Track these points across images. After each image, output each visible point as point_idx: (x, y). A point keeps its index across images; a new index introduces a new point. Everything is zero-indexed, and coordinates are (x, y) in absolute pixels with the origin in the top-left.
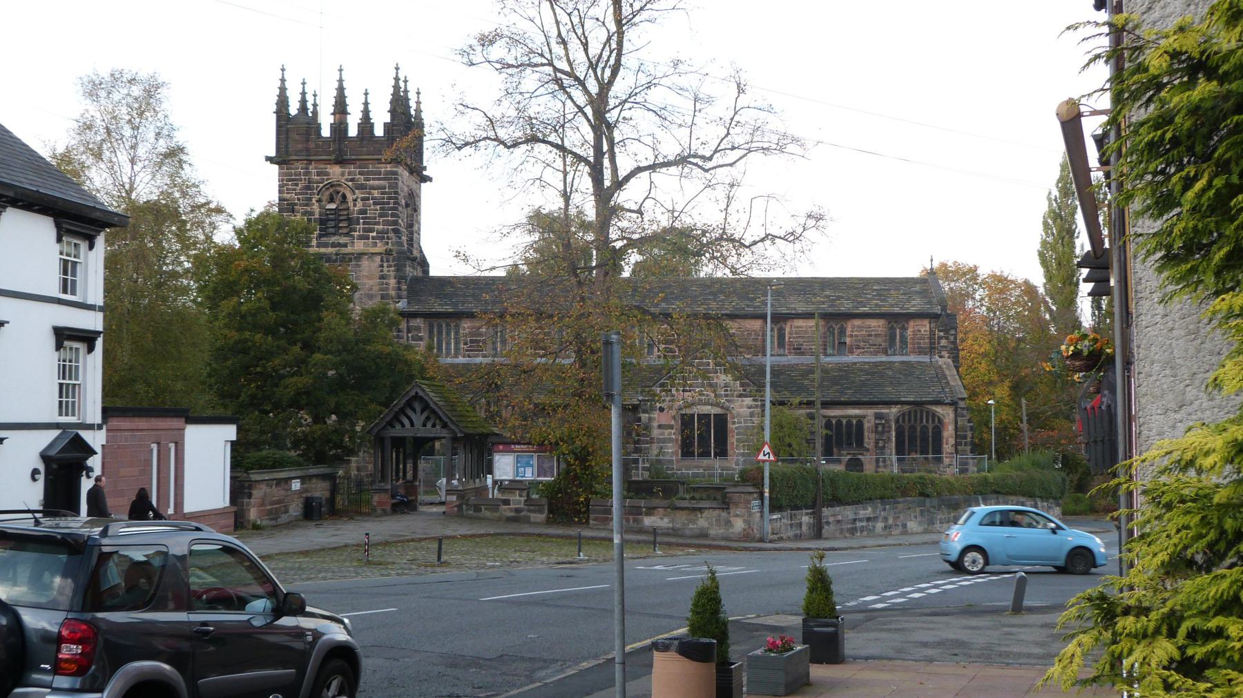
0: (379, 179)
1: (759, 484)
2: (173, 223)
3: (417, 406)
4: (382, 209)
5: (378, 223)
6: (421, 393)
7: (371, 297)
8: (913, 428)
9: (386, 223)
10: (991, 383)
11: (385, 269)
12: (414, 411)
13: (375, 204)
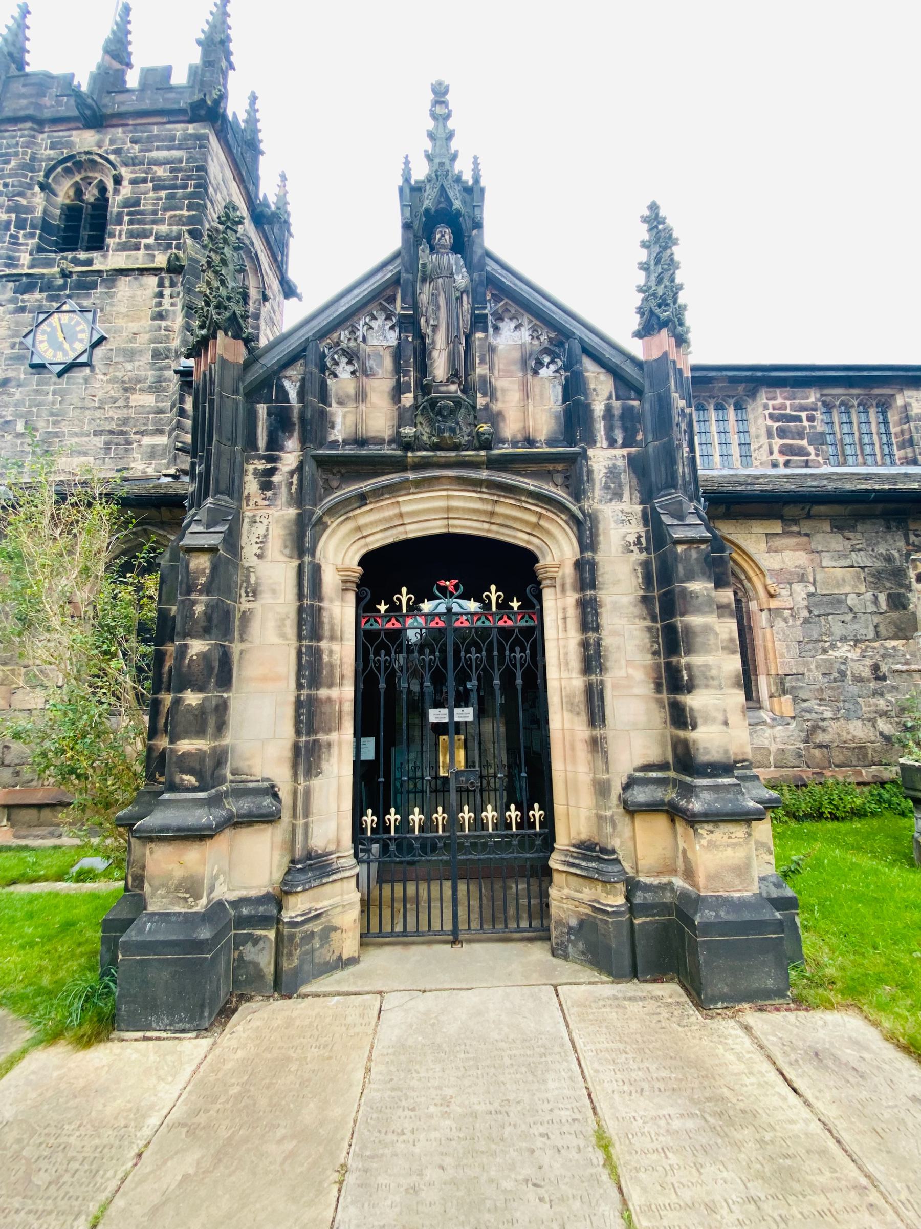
0: (169, 148)
4: (170, 197)
5: (161, 221)
7: (130, 355)
9: (180, 221)
11: (166, 301)
13: (156, 188)
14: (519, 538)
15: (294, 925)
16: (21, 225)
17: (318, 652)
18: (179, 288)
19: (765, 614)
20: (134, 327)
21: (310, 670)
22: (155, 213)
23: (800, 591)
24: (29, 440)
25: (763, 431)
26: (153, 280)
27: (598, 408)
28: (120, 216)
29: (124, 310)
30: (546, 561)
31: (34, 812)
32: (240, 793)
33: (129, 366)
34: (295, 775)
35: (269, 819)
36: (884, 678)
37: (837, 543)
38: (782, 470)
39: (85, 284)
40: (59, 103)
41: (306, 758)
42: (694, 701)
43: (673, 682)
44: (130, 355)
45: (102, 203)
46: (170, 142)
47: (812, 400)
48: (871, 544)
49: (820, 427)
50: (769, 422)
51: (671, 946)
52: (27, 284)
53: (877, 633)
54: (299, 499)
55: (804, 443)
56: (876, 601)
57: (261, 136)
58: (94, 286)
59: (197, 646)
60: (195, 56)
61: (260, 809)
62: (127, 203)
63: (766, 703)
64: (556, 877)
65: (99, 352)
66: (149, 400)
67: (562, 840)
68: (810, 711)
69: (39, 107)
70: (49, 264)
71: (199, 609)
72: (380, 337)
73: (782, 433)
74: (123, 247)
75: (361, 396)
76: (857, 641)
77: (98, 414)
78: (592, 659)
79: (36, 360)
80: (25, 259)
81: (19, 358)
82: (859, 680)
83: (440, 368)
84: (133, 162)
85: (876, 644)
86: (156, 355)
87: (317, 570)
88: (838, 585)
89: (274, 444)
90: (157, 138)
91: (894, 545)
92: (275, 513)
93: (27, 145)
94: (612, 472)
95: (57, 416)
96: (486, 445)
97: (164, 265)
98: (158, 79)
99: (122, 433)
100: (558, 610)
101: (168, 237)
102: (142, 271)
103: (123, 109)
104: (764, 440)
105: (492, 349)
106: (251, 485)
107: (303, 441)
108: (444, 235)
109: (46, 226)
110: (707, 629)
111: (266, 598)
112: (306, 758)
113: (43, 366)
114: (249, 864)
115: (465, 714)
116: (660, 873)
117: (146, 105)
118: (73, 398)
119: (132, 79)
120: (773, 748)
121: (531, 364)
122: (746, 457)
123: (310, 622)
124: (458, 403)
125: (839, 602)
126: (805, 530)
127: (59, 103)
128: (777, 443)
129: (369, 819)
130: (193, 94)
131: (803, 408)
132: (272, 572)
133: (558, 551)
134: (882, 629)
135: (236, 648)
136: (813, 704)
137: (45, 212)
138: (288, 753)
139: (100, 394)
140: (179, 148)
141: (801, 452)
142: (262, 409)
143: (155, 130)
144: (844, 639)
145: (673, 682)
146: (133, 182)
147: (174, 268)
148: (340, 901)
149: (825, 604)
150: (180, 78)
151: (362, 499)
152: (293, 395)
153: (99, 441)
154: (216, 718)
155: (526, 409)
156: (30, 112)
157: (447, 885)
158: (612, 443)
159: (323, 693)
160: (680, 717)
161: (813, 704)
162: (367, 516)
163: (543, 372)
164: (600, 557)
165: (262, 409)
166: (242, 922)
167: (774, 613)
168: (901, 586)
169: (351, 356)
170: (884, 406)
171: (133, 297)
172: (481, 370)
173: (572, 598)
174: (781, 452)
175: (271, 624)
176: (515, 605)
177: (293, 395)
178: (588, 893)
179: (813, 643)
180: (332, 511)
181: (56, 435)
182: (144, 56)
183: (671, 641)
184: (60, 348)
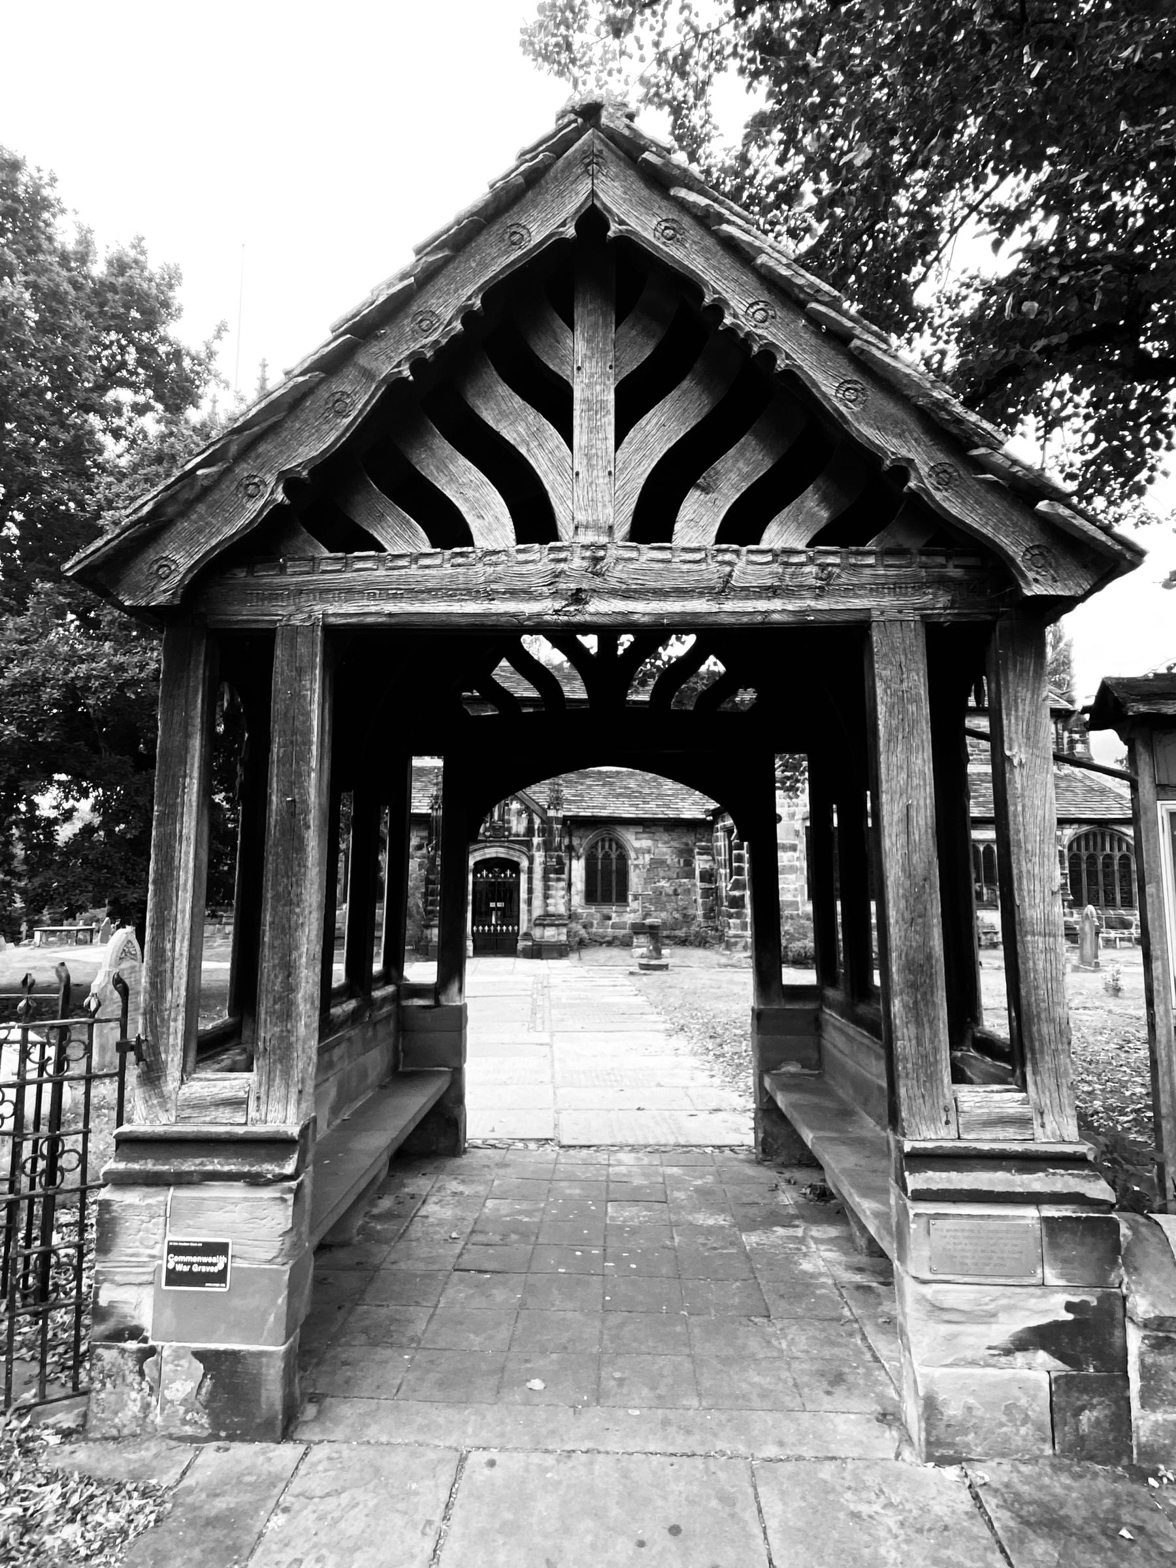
1: (955, 1336)
2: (800, 42)
3: (590, 367)
6: (636, 217)
8: (1092, 859)
10: (682, 1207)
12: (555, 404)
37: (666, 837)
43: (546, 897)
48: (680, 837)
51: (538, 951)
78: (530, 891)
82: (667, 895)
83: (496, 817)
91: (689, 839)
100: (524, 878)
115: (499, 905)
121: (519, 813)
133: (525, 864)
149: (657, 863)
167: (636, 866)
179: (649, 880)
183: (547, 888)
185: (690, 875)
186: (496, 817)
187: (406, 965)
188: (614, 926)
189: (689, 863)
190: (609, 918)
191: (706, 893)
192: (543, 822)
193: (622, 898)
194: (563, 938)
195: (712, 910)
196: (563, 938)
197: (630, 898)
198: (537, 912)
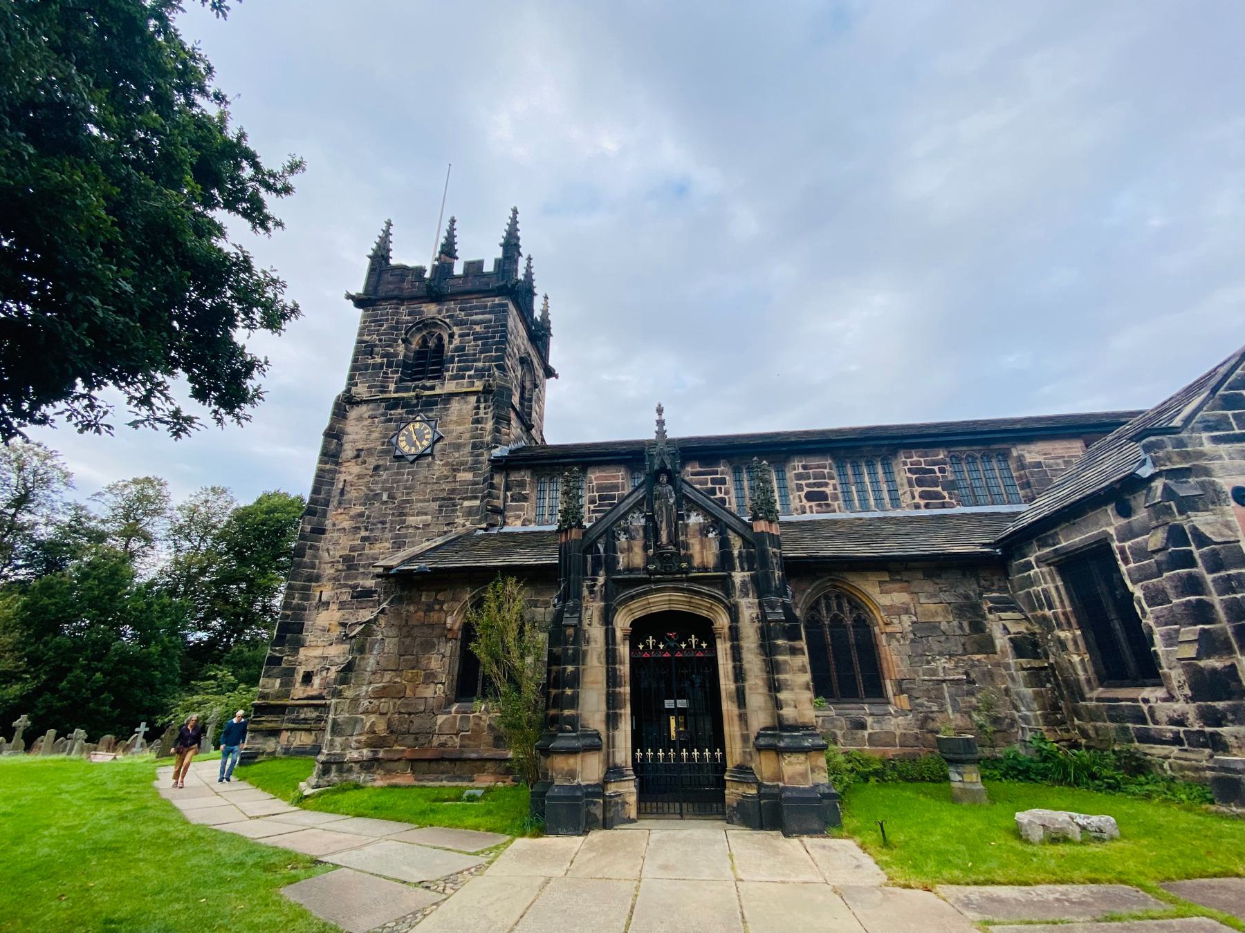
5: (478, 360)
7: (458, 447)
9: (490, 359)
11: (482, 411)
13: (475, 339)
14: (704, 613)
15: (610, 796)
16: (389, 365)
17: (615, 669)
18: (490, 403)
19: (884, 636)
20: (461, 429)
21: (612, 679)
22: (475, 355)
23: (906, 620)
24: (390, 506)
25: (905, 481)
26: (473, 399)
27: (736, 553)
28: (453, 357)
29: (454, 418)
30: (717, 625)
31: (426, 764)
32: (585, 736)
33: (457, 455)
34: (608, 729)
35: (597, 748)
36: (973, 682)
37: (929, 587)
38: (924, 512)
39: (430, 403)
40: (413, 286)
41: (612, 720)
42: (782, 696)
43: (774, 687)
44: (458, 447)
45: (440, 346)
46: (483, 309)
47: (941, 456)
49: (951, 477)
50: (909, 475)
51: (775, 813)
52: (393, 404)
53: (965, 649)
54: (605, 598)
55: (939, 489)
56: (961, 627)
57: (535, 284)
58: (436, 404)
59: (570, 668)
60: (499, 253)
61: (592, 744)
62: (457, 349)
63: (892, 700)
64: (728, 784)
65: (438, 446)
66: (469, 476)
67: (730, 766)
68: (921, 705)
69: (401, 289)
70: (407, 390)
71: (570, 652)
72: (638, 521)
73: (920, 483)
74: (453, 378)
75: (630, 549)
76: (951, 655)
77: (435, 487)
78: (739, 675)
79: (398, 453)
80: (392, 387)
81: (386, 452)
83: (664, 538)
84: (460, 323)
85: (965, 658)
86: (474, 446)
87: (614, 630)
88: (933, 616)
89: (595, 573)
90: (476, 307)
91: (971, 588)
92: (596, 605)
93: (393, 314)
94: (744, 583)
95: (410, 489)
96: (686, 572)
97: (481, 389)
98: (474, 268)
99: (451, 499)
100: (723, 648)
101: (483, 369)
102: (467, 394)
103: (455, 289)
104: (907, 488)
105: (687, 525)
106: (586, 592)
107: (607, 573)
108: (664, 479)
109: (405, 365)
110: (786, 662)
111: (593, 645)
112: (612, 720)
113: (402, 457)
114: (590, 769)
115: (682, 703)
116: (773, 780)
117: (469, 286)
118: (421, 476)
119: (458, 269)
120: (898, 732)
121: (703, 531)
122: (895, 502)
123: (611, 656)
124: (673, 554)
125: (935, 627)
126: (905, 578)
127: (413, 286)
128: (918, 490)
129: (639, 754)
130: (498, 280)
131: (935, 463)
132: (596, 632)
133: (722, 621)
134: (969, 648)
135: (581, 667)
136: (923, 700)
137: (405, 356)
138: (603, 718)
139: (437, 474)
140: (489, 313)
141: (938, 496)
142: (589, 557)
143: (475, 303)
144: (941, 654)
145: (774, 687)
146: (461, 336)
147: (487, 391)
148: (628, 789)
149: (924, 630)
150: (489, 267)
151: (632, 598)
152: (602, 550)
153: (435, 505)
154: (574, 702)
155: (704, 552)
156: (395, 293)
157: (677, 805)
158: (743, 570)
159: (618, 689)
160: (778, 705)
161: (923, 700)
162: (634, 605)
163: (710, 535)
164: (740, 624)
165: (589, 557)
166: (588, 795)
167: (891, 635)
168: (978, 615)
169: (626, 531)
170: (1005, 456)
171: (460, 410)
172: (682, 538)
173: (728, 645)
174: (921, 497)
175: (595, 657)
176: (704, 645)
177: (602, 550)
178: (741, 789)
179: (918, 657)
180: (620, 604)
181: (408, 501)
182: (465, 255)
183: (772, 668)
184: (414, 444)
185: (987, 646)
186: (664, 538)
187: (550, 441)
188: (872, 740)
189: (978, 627)
190: (863, 726)
191: (1036, 677)
192: (746, 543)
193: (875, 690)
194: (823, 778)
195: (1056, 708)
196: (823, 778)
197: (890, 688)
198: (759, 719)
